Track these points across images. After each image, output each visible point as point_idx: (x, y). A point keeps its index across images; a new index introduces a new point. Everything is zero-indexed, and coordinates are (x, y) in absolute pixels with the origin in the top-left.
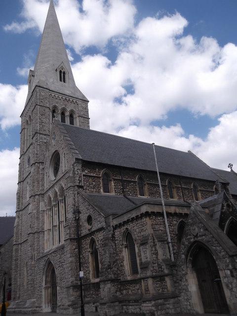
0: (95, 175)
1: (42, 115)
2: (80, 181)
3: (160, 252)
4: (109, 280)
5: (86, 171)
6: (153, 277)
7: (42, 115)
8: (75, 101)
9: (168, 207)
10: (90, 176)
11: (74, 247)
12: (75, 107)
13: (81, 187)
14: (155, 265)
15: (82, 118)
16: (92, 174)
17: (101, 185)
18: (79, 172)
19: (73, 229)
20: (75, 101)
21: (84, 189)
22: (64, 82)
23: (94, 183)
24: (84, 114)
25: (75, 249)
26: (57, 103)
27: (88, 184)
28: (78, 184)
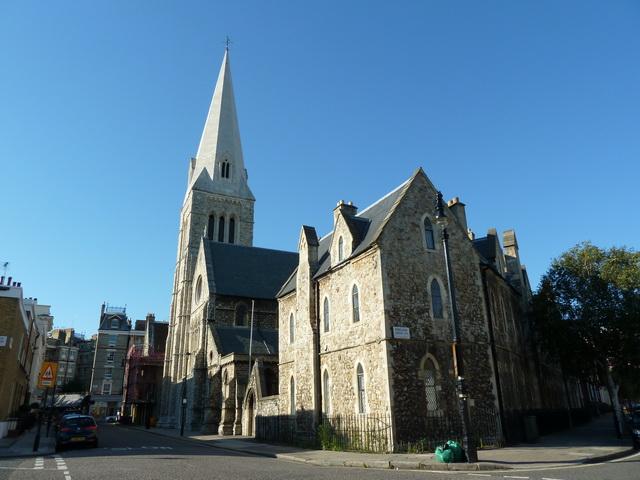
22: (227, 177)
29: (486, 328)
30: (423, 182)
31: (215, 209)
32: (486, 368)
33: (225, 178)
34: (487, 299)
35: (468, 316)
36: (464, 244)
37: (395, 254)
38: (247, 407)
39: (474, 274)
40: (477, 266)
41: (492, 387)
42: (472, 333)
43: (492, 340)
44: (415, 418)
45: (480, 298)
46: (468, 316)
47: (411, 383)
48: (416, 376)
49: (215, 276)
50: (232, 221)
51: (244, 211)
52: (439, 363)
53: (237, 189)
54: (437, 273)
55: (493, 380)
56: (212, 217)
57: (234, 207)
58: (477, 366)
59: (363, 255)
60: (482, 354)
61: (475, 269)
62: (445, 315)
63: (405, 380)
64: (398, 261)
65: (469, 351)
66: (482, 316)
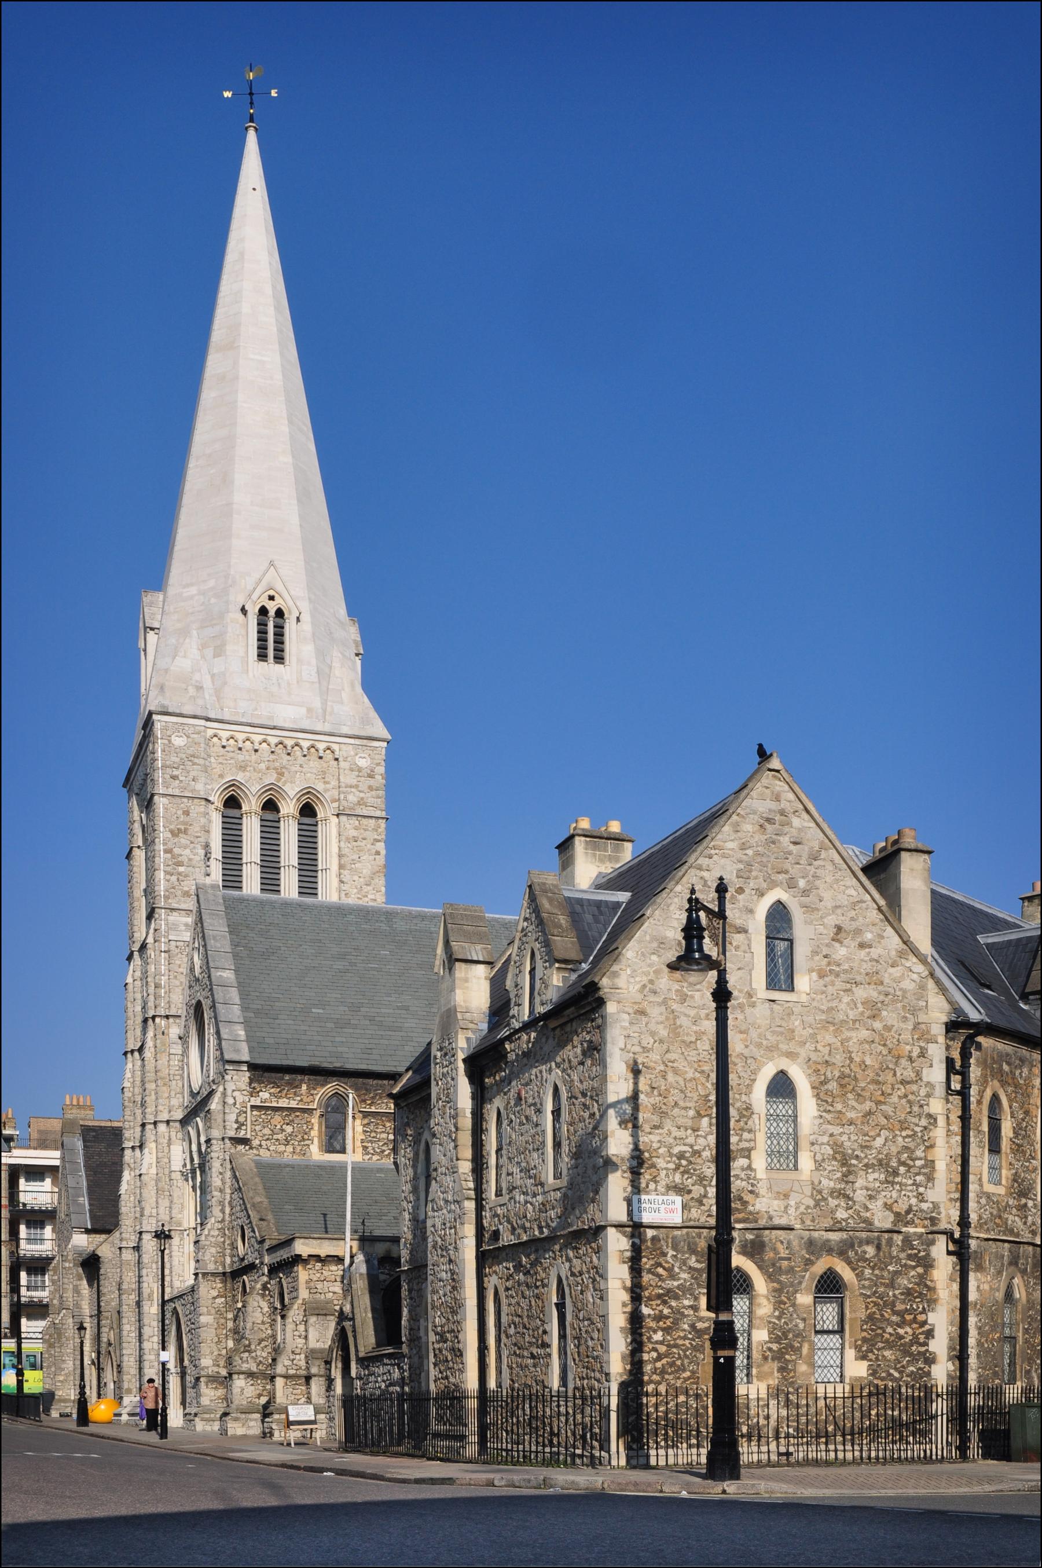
0: (293, 1104)
1: (175, 833)
2: (240, 1125)
3: (313, 1335)
4: (243, 1373)
5: (265, 1095)
6: (286, 1377)
7: (175, 833)
8: (321, 746)
9: (367, 1243)
10: (276, 1109)
11: (215, 1293)
12: (323, 775)
13: (244, 1141)
14: (298, 1357)
15: (354, 821)
16: (283, 1103)
17: (314, 1133)
18: (240, 1098)
19: (213, 1250)
20: (321, 746)
21: (251, 1148)
22: (279, 659)
23: (289, 1129)
24: (361, 802)
25: (215, 1298)
26: (243, 768)
27: (267, 1131)
28: (232, 1133)
29: (941, 1193)
30: (777, 798)
31: (240, 777)
32: (923, 1293)
33: (271, 667)
34: (965, 1118)
35: (882, 1164)
36: (896, 972)
37: (656, 1013)
38: (340, 1365)
39: (923, 1054)
40: (938, 1030)
41: (930, 1334)
42: (888, 1207)
43: (964, 1222)
44: (682, 1398)
45: (932, 1118)
46: (882, 1164)
47: (676, 1322)
48: (695, 1308)
49: (245, 1009)
50: (308, 811)
51: (349, 778)
52: (770, 1277)
53: (317, 704)
54: (791, 1055)
55: (941, 1320)
56: (232, 803)
57: (314, 764)
58: (892, 1285)
59: (570, 1011)
60: (910, 1257)
61: (922, 1034)
62: (806, 1162)
63: (659, 1317)
64: (663, 1032)
65: (870, 1251)
66: (931, 1164)
